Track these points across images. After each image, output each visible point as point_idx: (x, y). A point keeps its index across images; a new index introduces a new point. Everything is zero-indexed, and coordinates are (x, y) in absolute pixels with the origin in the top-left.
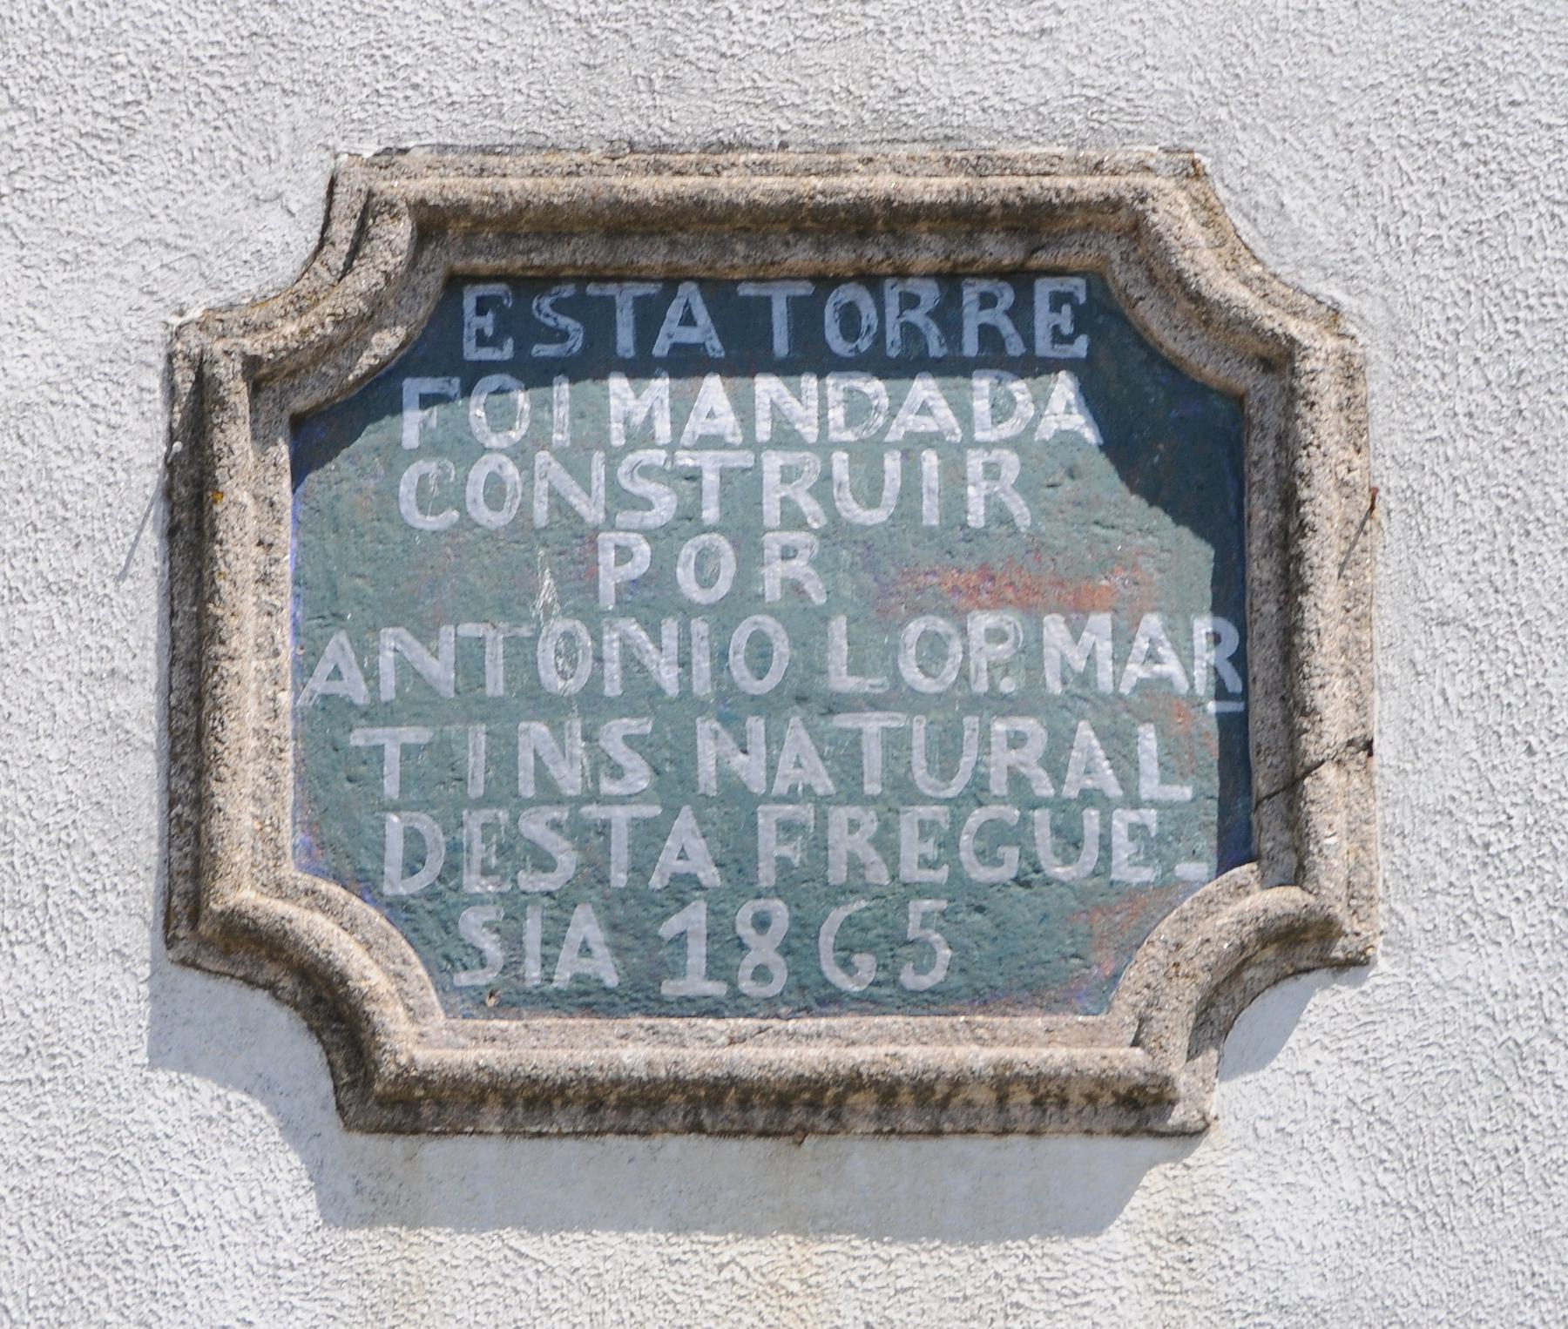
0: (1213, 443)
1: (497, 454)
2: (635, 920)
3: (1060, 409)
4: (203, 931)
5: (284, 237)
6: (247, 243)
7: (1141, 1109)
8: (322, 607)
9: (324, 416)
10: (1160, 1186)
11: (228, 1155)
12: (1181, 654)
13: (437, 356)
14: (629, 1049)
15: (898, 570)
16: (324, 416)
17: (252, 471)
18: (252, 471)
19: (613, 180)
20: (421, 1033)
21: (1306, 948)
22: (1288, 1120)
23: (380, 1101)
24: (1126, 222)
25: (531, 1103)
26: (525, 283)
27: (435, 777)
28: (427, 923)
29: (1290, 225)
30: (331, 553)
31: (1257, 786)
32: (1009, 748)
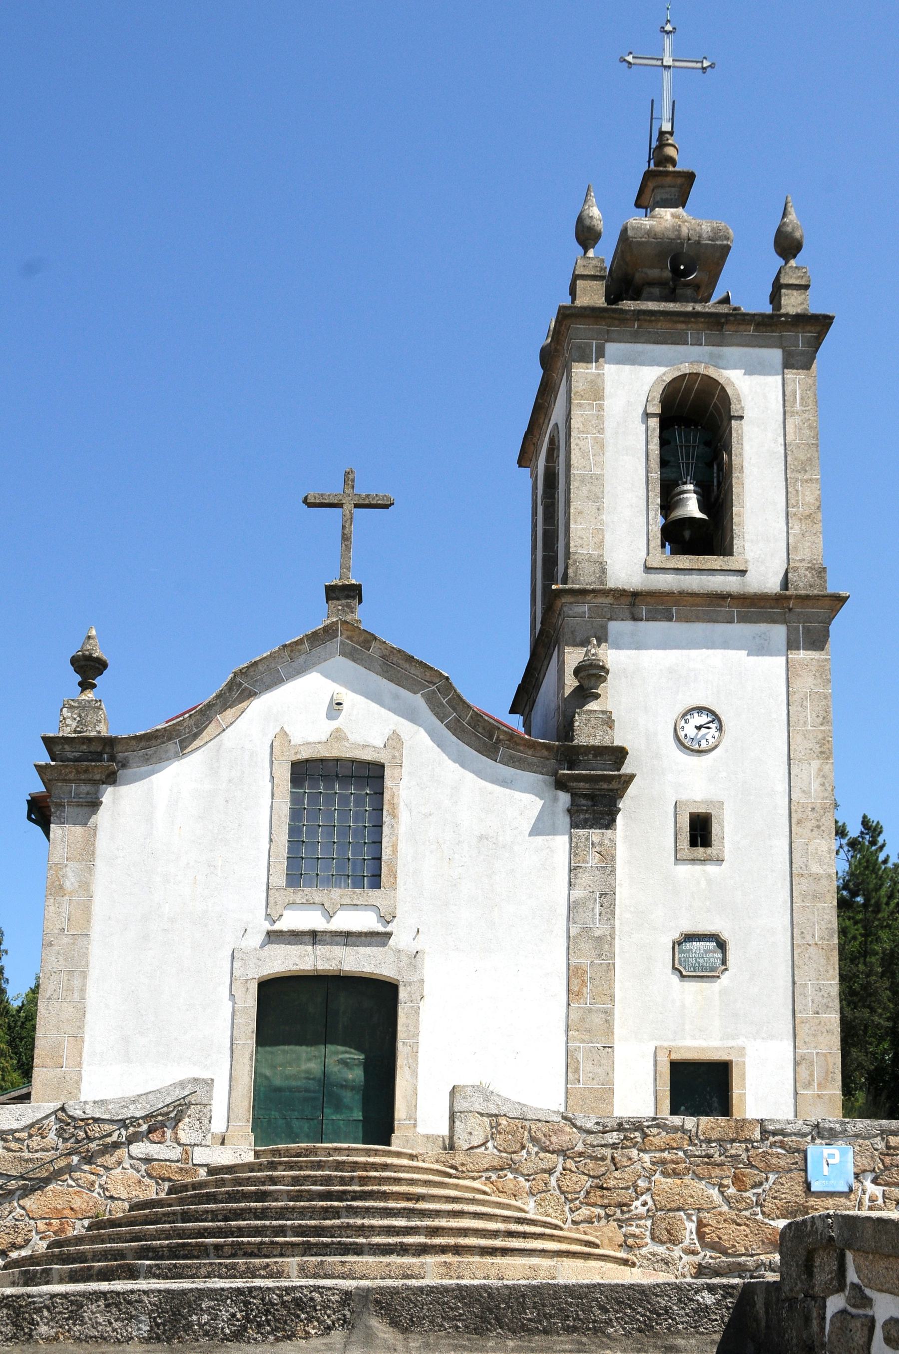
0: (722, 945)
1: (688, 946)
2: (694, 968)
3: (715, 944)
4: (674, 968)
5: (678, 935)
6: (676, 936)
7: (718, 977)
8: (679, 953)
9: (680, 943)
10: (719, 981)
11: (675, 979)
12: (720, 956)
13: (685, 941)
14: (694, 974)
15: (706, 952)
16: (680, 943)
17: (677, 946)
18: (677, 946)
19: (762, 1257)
20: (684, 973)
21: (726, 969)
22: (725, 978)
23: (682, 976)
24: (718, 935)
25: (689, 976)
26: (690, 937)
27: (685, 961)
28: (685, 968)
29: (725, 936)
30: (52, 1332)
31: (724, 962)
32: (712, 960)
